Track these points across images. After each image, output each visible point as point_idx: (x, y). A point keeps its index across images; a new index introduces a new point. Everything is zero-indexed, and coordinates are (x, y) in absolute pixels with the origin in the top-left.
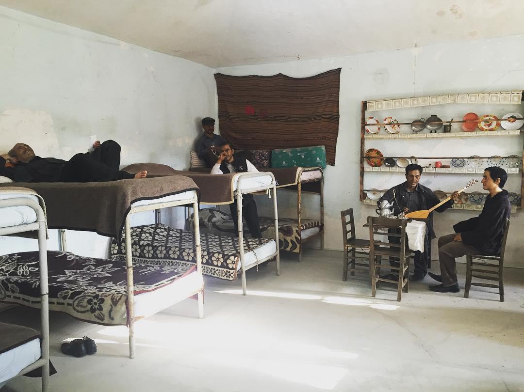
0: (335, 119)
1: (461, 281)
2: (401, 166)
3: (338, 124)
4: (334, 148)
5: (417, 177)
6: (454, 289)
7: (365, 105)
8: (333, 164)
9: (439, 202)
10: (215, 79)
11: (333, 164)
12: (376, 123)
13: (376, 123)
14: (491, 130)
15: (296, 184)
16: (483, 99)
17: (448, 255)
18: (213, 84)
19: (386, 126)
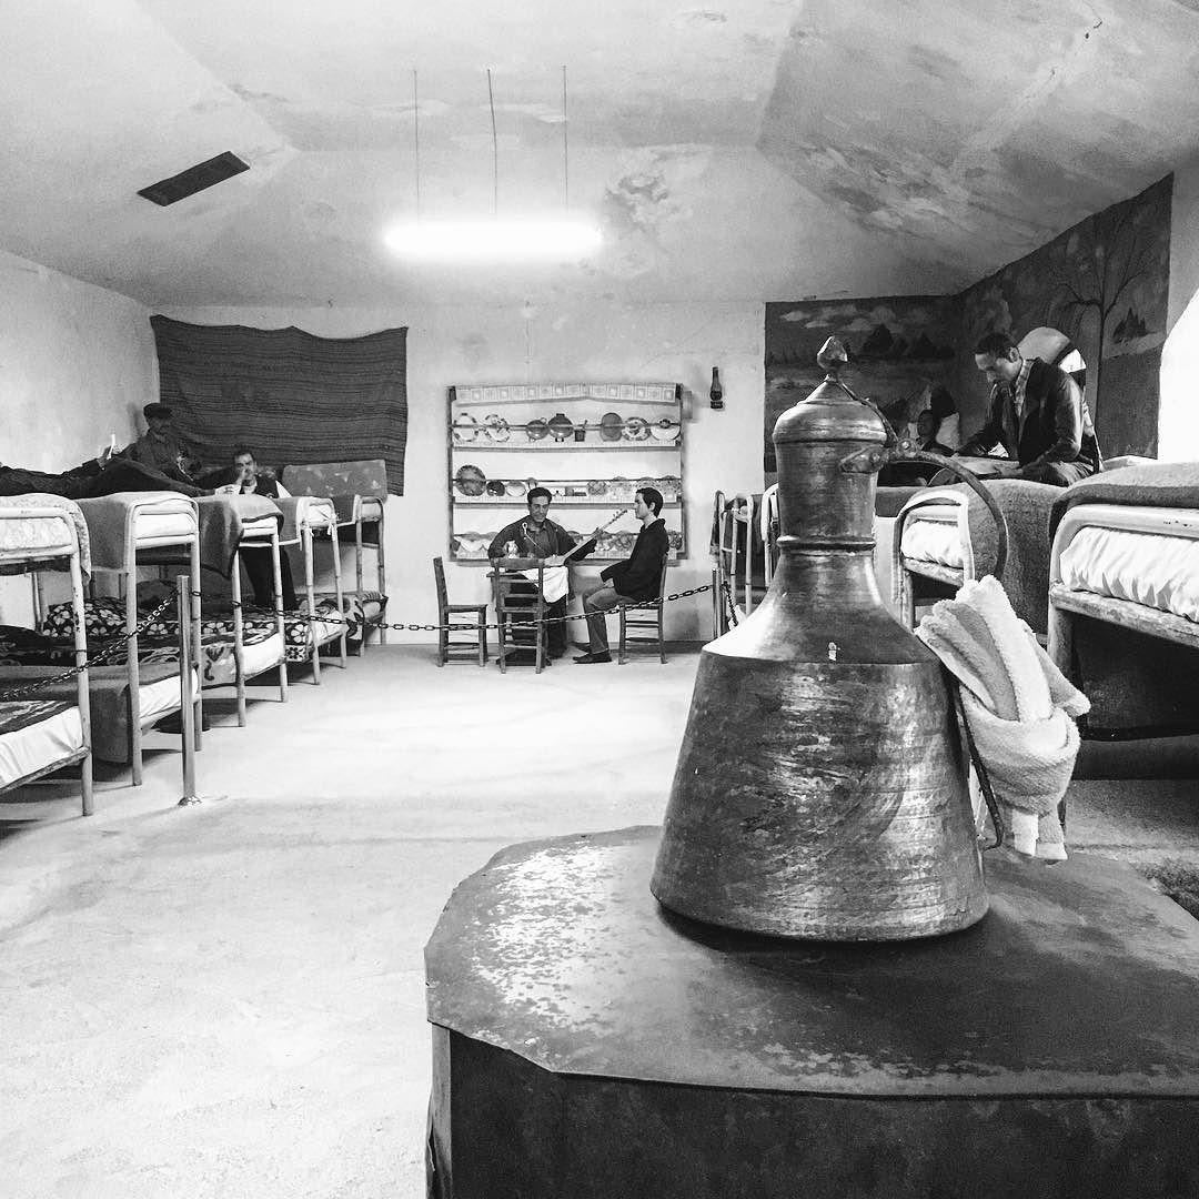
0: (400, 414)
2: (517, 495)
7: (452, 393)
8: (400, 493)
9: (575, 545)
11: (400, 493)
12: (471, 423)
13: (471, 423)
14: (639, 439)
15: (353, 522)
16: (627, 392)
18: (150, 332)
19: (489, 430)
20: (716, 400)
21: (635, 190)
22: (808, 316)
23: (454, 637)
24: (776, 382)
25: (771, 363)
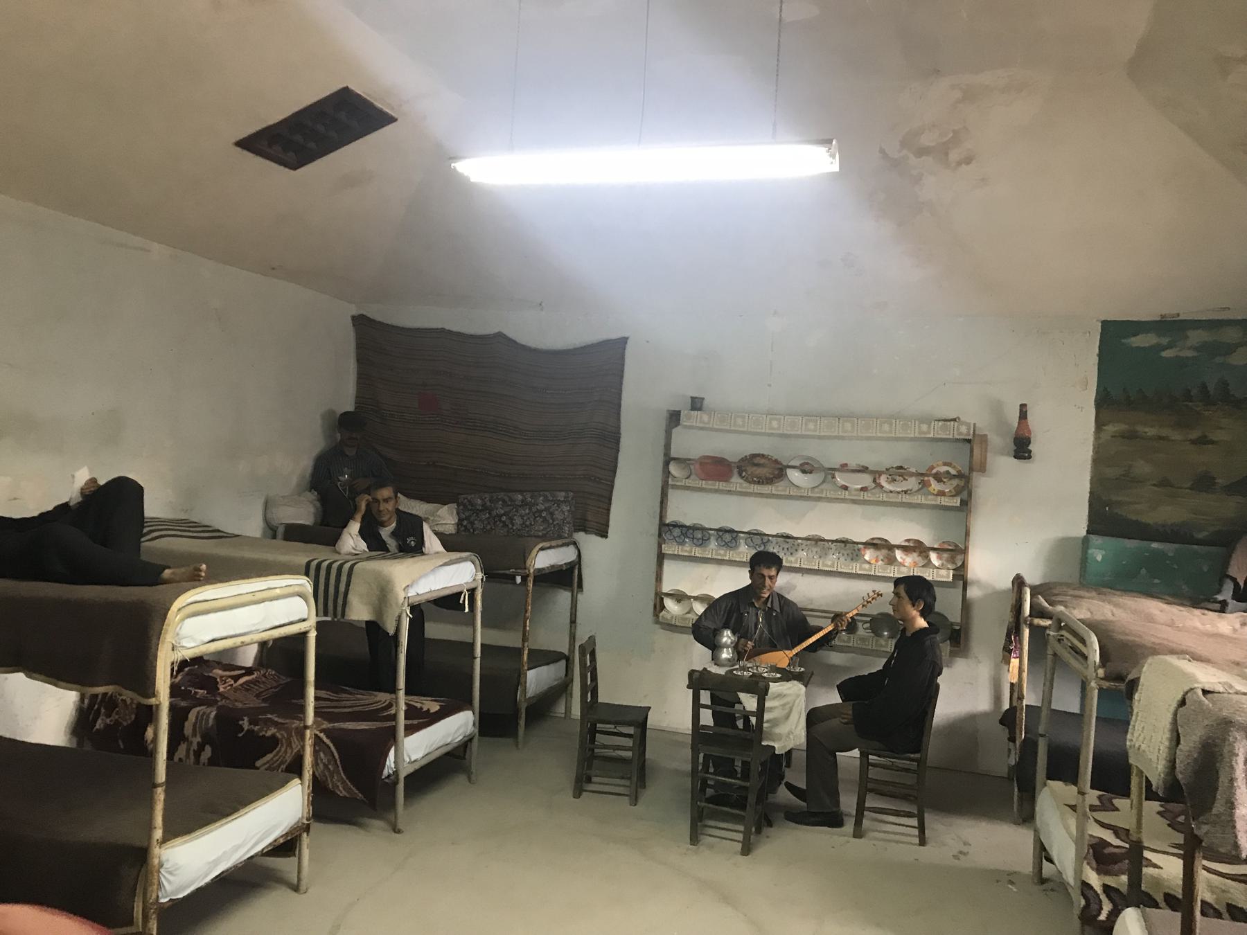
1: (848, 802)
3: (618, 451)
4: (607, 501)
5: (770, 577)
6: (834, 820)
10: (354, 325)
17: (791, 641)
20: (1021, 448)
21: (922, 152)
22: (1165, 341)
23: (914, 822)
24: (1111, 429)
25: (1104, 402)
